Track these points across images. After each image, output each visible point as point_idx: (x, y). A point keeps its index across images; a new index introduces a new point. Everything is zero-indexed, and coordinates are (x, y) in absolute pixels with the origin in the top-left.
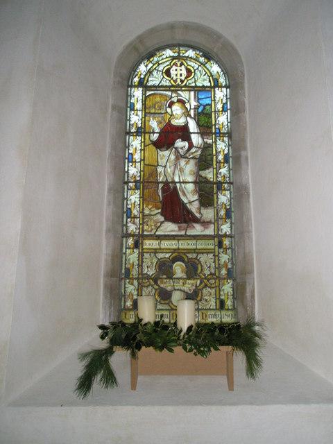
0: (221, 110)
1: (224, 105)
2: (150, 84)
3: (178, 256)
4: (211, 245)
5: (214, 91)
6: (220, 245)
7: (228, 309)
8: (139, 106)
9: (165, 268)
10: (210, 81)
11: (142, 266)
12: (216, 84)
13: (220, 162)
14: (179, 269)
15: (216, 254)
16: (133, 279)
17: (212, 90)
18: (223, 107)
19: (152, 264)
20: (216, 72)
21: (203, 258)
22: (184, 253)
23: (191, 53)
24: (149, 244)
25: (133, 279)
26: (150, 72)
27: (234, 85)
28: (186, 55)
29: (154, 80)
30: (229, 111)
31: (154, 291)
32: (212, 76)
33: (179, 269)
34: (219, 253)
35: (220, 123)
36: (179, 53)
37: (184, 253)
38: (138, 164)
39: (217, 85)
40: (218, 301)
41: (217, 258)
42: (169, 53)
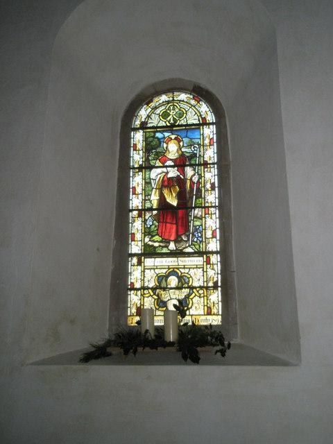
0: (208, 144)
1: (214, 232)
2: (149, 125)
3: (173, 272)
4: (199, 261)
5: (203, 128)
6: (208, 262)
7: (214, 314)
8: (139, 190)
9: (162, 279)
10: (199, 120)
11: (144, 280)
12: (209, 311)
13: (208, 190)
14: (173, 281)
15: (205, 270)
16: (138, 194)
17: (201, 127)
18: (210, 143)
19: (155, 242)
20: (204, 111)
21: (192, 272)
22: (178, 269)
23: (183, 96)
24: (149, 262)
25: (138, 194)
26: (149, 116)
27: (220, 124)
28: (179, 98)
29: (155, 121)
30: (220, 289)
31: (153, 300)
32: (201, 115)
33: (173, 281)
34: (207, 269)
35: (209, 201)
36: (173, 98)
37: (178, 269)
38: (140, 196)
39: (204, 123)
40: (206, 307)
41: (205, 273)
42: (164, 98)
